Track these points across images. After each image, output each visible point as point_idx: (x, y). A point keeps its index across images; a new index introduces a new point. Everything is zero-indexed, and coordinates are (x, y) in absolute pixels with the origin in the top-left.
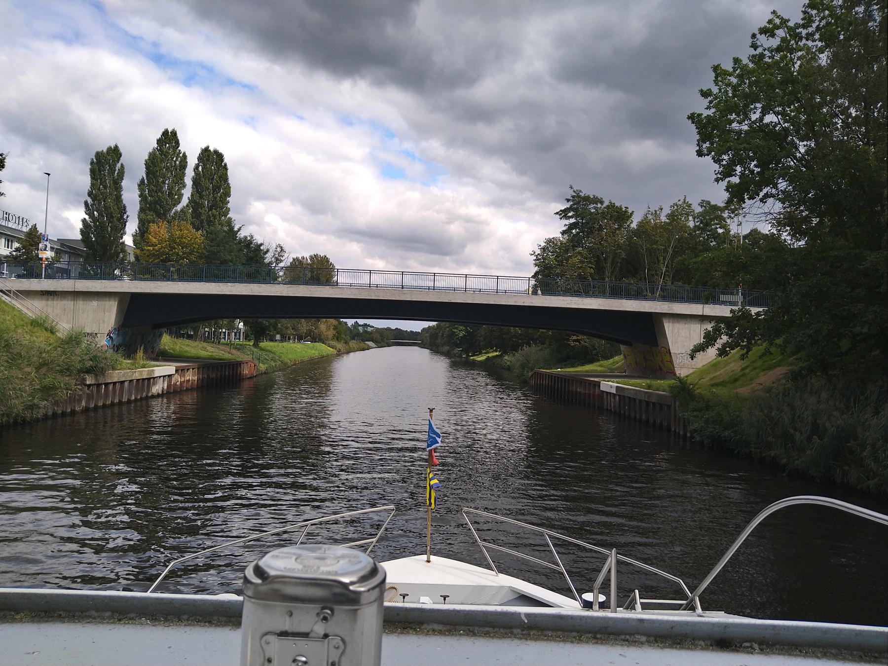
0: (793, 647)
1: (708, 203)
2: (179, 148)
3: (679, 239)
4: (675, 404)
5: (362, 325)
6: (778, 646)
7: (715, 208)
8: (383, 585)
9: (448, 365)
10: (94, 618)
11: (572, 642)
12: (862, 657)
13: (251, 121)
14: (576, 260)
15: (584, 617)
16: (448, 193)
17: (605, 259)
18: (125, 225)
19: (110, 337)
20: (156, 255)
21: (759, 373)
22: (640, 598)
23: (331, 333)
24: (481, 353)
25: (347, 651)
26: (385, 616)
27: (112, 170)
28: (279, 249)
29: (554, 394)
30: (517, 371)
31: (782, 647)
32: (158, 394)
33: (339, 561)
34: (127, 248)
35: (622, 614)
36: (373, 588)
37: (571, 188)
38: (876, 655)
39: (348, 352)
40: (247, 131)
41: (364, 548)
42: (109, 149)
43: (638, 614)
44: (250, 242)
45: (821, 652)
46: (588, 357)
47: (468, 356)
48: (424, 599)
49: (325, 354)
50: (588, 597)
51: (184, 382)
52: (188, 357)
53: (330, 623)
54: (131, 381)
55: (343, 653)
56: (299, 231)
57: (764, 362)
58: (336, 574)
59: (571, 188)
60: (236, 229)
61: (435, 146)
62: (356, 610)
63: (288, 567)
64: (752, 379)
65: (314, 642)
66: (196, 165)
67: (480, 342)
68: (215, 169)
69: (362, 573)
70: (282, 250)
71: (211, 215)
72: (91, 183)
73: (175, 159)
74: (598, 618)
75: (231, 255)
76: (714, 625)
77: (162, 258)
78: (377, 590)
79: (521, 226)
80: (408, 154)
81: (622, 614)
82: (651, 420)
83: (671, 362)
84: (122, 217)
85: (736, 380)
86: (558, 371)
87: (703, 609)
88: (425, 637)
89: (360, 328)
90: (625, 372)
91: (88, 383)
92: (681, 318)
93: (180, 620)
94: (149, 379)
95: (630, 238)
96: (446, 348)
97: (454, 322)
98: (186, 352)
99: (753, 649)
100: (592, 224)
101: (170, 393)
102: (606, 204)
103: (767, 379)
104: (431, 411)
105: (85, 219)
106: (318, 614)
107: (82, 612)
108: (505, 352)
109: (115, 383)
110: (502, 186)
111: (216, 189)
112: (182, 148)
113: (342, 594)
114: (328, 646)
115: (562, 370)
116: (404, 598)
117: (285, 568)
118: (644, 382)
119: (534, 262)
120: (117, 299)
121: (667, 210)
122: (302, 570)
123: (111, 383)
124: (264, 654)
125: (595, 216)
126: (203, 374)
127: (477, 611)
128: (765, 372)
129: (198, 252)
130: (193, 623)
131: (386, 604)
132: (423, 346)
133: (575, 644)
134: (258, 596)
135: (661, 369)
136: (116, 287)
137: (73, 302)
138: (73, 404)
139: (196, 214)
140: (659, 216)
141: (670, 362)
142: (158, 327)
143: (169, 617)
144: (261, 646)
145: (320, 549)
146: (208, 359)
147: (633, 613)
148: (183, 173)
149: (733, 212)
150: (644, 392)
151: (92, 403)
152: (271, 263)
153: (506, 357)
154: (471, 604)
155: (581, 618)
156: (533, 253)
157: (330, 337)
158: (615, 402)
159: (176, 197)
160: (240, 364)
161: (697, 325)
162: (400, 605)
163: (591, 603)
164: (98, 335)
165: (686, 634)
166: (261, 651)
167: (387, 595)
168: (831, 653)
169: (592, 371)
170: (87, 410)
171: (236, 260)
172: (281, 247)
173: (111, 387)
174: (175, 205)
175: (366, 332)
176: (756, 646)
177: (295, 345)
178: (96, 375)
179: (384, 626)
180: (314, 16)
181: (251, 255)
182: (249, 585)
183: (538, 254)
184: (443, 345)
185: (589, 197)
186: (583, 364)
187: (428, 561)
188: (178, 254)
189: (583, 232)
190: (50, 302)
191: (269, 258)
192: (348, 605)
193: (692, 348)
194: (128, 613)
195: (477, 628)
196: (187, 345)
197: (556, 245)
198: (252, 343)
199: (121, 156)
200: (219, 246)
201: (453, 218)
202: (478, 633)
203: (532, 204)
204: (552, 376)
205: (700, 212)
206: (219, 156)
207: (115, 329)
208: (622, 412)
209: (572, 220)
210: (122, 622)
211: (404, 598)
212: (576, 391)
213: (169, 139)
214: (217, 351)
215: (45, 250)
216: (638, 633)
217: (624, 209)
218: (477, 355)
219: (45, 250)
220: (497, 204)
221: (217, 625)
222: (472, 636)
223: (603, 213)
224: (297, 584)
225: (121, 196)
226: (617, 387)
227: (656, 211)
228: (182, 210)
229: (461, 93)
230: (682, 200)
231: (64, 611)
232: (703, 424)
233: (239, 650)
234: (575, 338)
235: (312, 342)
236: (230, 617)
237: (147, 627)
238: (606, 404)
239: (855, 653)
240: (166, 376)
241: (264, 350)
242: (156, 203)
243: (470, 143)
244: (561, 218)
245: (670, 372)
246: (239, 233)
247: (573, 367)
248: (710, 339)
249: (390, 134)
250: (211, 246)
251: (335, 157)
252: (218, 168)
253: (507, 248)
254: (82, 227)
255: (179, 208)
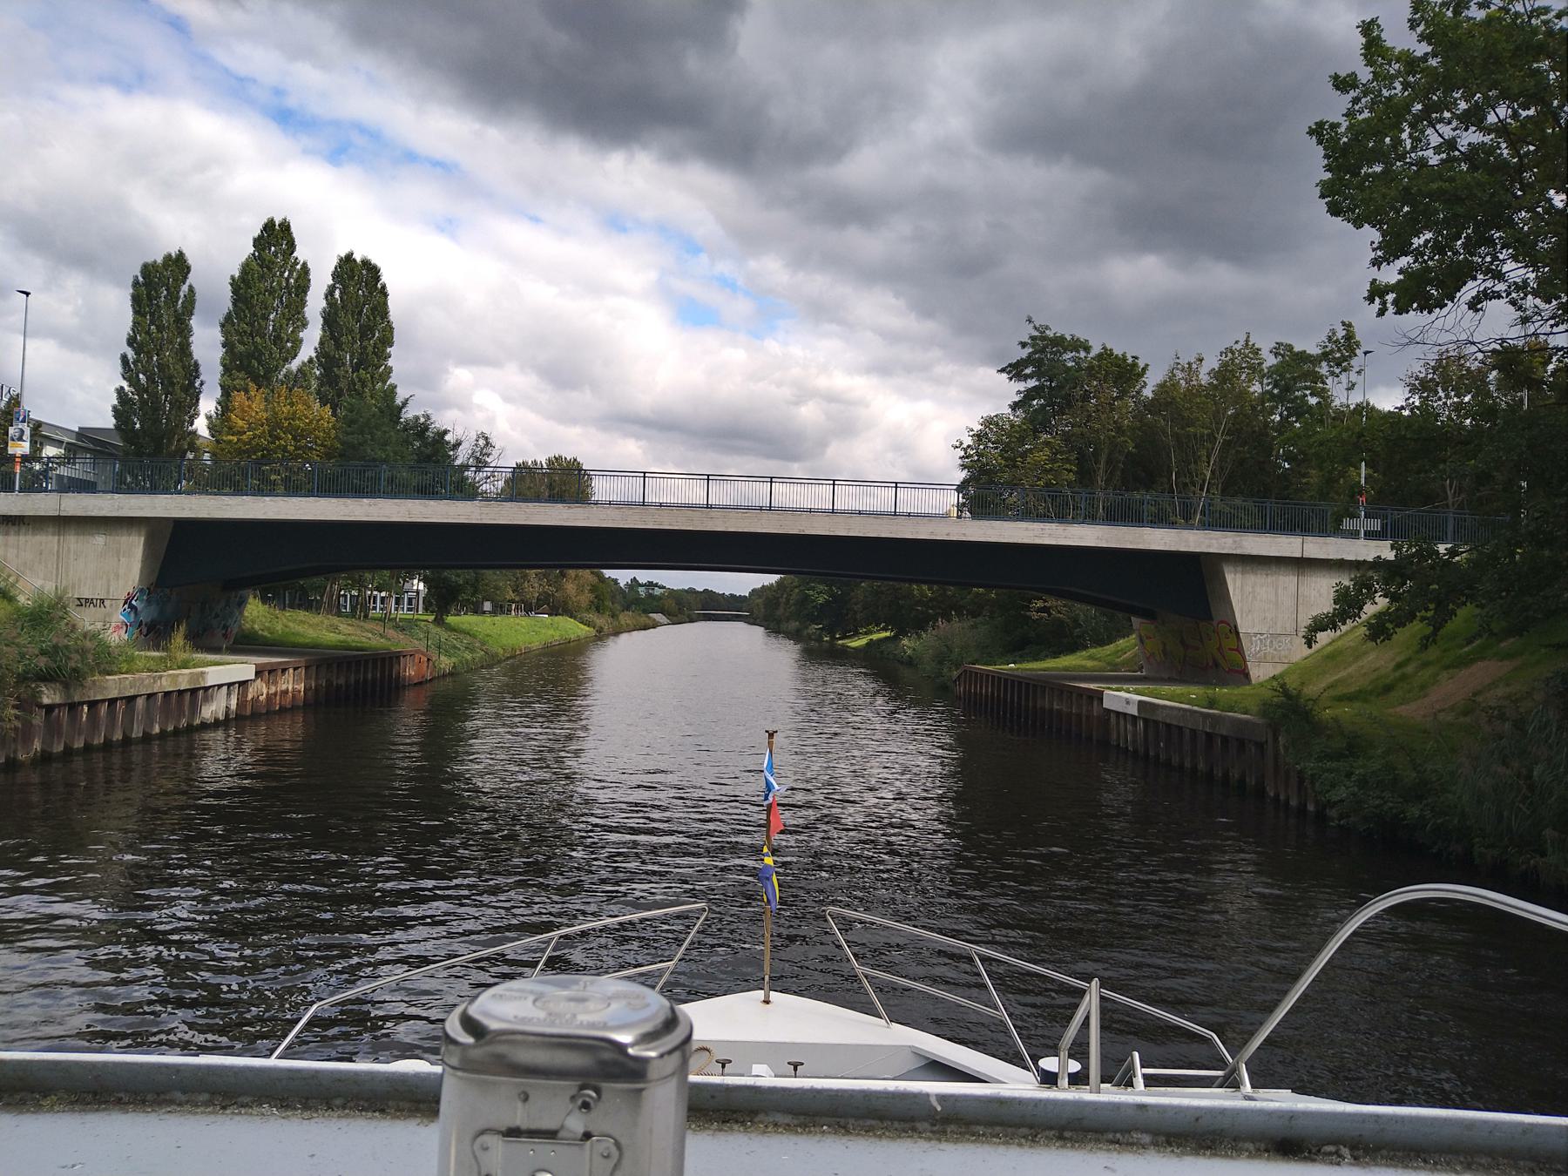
0: (1412, 1154)
1: (1290, 348)
2: (295, 254)
3: (1235, 416)
4: (1276, 740)
5: (645, 585)
6: (1384, 1152)
7: (1303, 357)
8: (687, 1047)
9: (797, 656)
10: (180, 1105)
11: (1020, 1145)
12: (1534, 1172)
13: (447, 226)
14: (1042, 456)
15: (1040, 1100)
16: (797, 351)
17: (1096, 454)
18: (198, 400)
19: (132, 607)
20: (244, 452)
21: (1438, 675)
22: (1142, 1067)
23: (586, 598)
24: (856, 634)
25: (626, 1162)
26: (690, 1099)
27: (173, 296)
28: (482, 442)
29: (1005, 713)
30: (928, 668)
31: (1392, 1153)
32: (217, 720)
33: (609, 1005)
34: (198, 442)
35: (1109, 1095)
36: (670, 1052)
37: (1030, 321)
38: (1559, 1166)
39: (617, 633)
40: (441, 243)
41: (647, 980)
42: (168, 258)
43: (1139, 1095)
44: (425, 428)
45: (1461, 1163)
46: (1063, 640)
47: (833, 638)
48: (757, 1069)
49: (573, 637)
50: (1049, 1064)
51: (275, 694)
52: (295, 645)
53: (594, 1114)
54: (150, 696)
55: (616, 1167)
56: (533, 419)
57: (1445, 651)
58: (605, 1027)
59: (1030, 321)
60: (399, 401)
61: (773, 268)
62: (641, 1090)
63: (521, 1014)
64: (1423, 687)
65: (566, 1147)
66: (329, 287)
67: (856, 613)
68: (364, 295)
69: (648, 1028)
70: (487, 443)
71: (356, 380)
72: (134, 322)
73: (286, 274)
74: (1065, 1103)
75: (385, 451)
76: (1271, 1114)
77: (254, 457)
78: (677, 1055)
79: (926, 407)
80: (726, 284)
81: (1109, 1095)
82: (1218, 773)
83: (1239, 650)
84: (192, 384)
85: (1388, 689)
86: (1011, 669)
87: (1253, 1087)
88: (760, 1137)
89: (640, 589)
90: (1141, 669)
91: (46, 701)
92: (1260, 563)
93: (330, 1107)
94: (194, 691)
95: (1139, 416)
96: (794, 625)
97: (808, 573)
98: (298, 634)
99: (1340, 1156)
100: (1070, 389)
101: (237, 721)
102: (1096, 350)
103: (1452, 688)
104: (771, 735)
105: (122, 388)
106: (573, 1098)
107: (158, 1094)
108: (901, 632)
109: (112, 702)
110: (891, 337)
111: (366, 332)
112: (301, 253)
113: (615, 1063)
114: (591, 1151)
115: (1018, 666)
116: (723, 1067)
117: (515, 1017)
118: (1195, 691)
119: (960, 461)
120: (143, 533)
121: (1212, 362)
122: (545, 1020)
123: (103, 701)
124: (479, 1167)
125: (1077, 374)
126: (317, 679)
127: (853, 1091)
128: (1451, 671)
129: (325, 446)
130: (352, 1113)
131: (692, 1078)
132: (752, 620)
133: (1026, 1149)
134: (468, 1066)
135: (1216, 665)
136: (142, 509)
137: (56, 538)
138: (13, 746)
139: (329, 378)
140: (1197, 372)
141: (1237, 650)
142: (235, 587)
143: (310, 1103)
144: (473, 1153)
145: (576, 982)
146: (335, 647)
147: (1129, 1094)
148: (302, 300)
149: (1338, 365)
150: (1201, 713)
151: (59, 743)
152: (466, 467)
153: (905, 642)
154: (842, 1078)
155: (1037, 1103)
156: (958, 444)
157: (584, 605)
158: (1135, 734)
159: (289, 345)
160: (398, 658)
161: (1291, 577)
162: (716, 1080)
163: (1056, 1075)
164: (106, 603)
165: (1222, 1130)
166: (473, 1161)
167: (694, 1062)
168: (1480, 1165)
169: (1075, 668)
170: (45, 758)
171: (396, 461)
172: (486, 438)
173: (104, 709)
174: (286, 360)
175: (651, 596)
176: (1345, 1151)
177: (517, 621)
178: (66, 686)
179: (688, 1117)
180: (559, 40)
181: (429, 451)
182: (452, 1047)
183: (969, 446)
184: (788, 619)
185: (1062, 338)
186: (1056, 654)
187: (767, 1002)
188: (285, 449)
189: (1052, 405)
190: (12, 539)
191: (462, 456)
192: (625, 1082)
193: (1309, 622)
194: (239, 1096)
195: (852, 1121)
196: (301, 621)
197: (1003, 429)
198: (433, 617)
199: (189, 272)
200: (362, 433)
201: (804, 394)
202: (854, 1129)
203: (945, 369)
204: (999, 679)
205: (1273, 366)
206: (372, 271)
207: (141, 591)
208: (1152, 753)
209: (1032, 383)
210: (228, 1112)
211: (723, 1067)
212: (1051, 710)
213: (276, 237)
214: (359, 632)
215: (20, 439)
216: (1137, 1130)
217: (1130, 360)
218: (849, 637)
219: (20, 439)
220: (881, 369)
221: (395, 1117)
222: (843, 1135)
223: (1090, 368)
224: (534, 1045)
225: (189, 345)
226: (1140, 702)
227: (1189, 364)
228: (300, 370)
229: (819, 174)
230: (1242, 342)
231: (126, 1091)
232: (1356, 789)
233: (435, 1162)
234: (1040, 604)
235: (550, 615)
236: (419, 1102)
237: (272, 1118)
238: (1114, 736)
239: (1522, 1163)
240: (234, 683)
241: (455, 630)
242: (250, 356)
243: (835, 262)
244: (1011, 379)
245: (1237, 671)
246: (404, 410)
247: (1037, 660)
248: (1347, 605)
249: (692, 247)
250: (348, 434)
251: (595, 288)
252: (370, 293)
253: (900, 446)
254: (116, 402)
255: (294, 365)
